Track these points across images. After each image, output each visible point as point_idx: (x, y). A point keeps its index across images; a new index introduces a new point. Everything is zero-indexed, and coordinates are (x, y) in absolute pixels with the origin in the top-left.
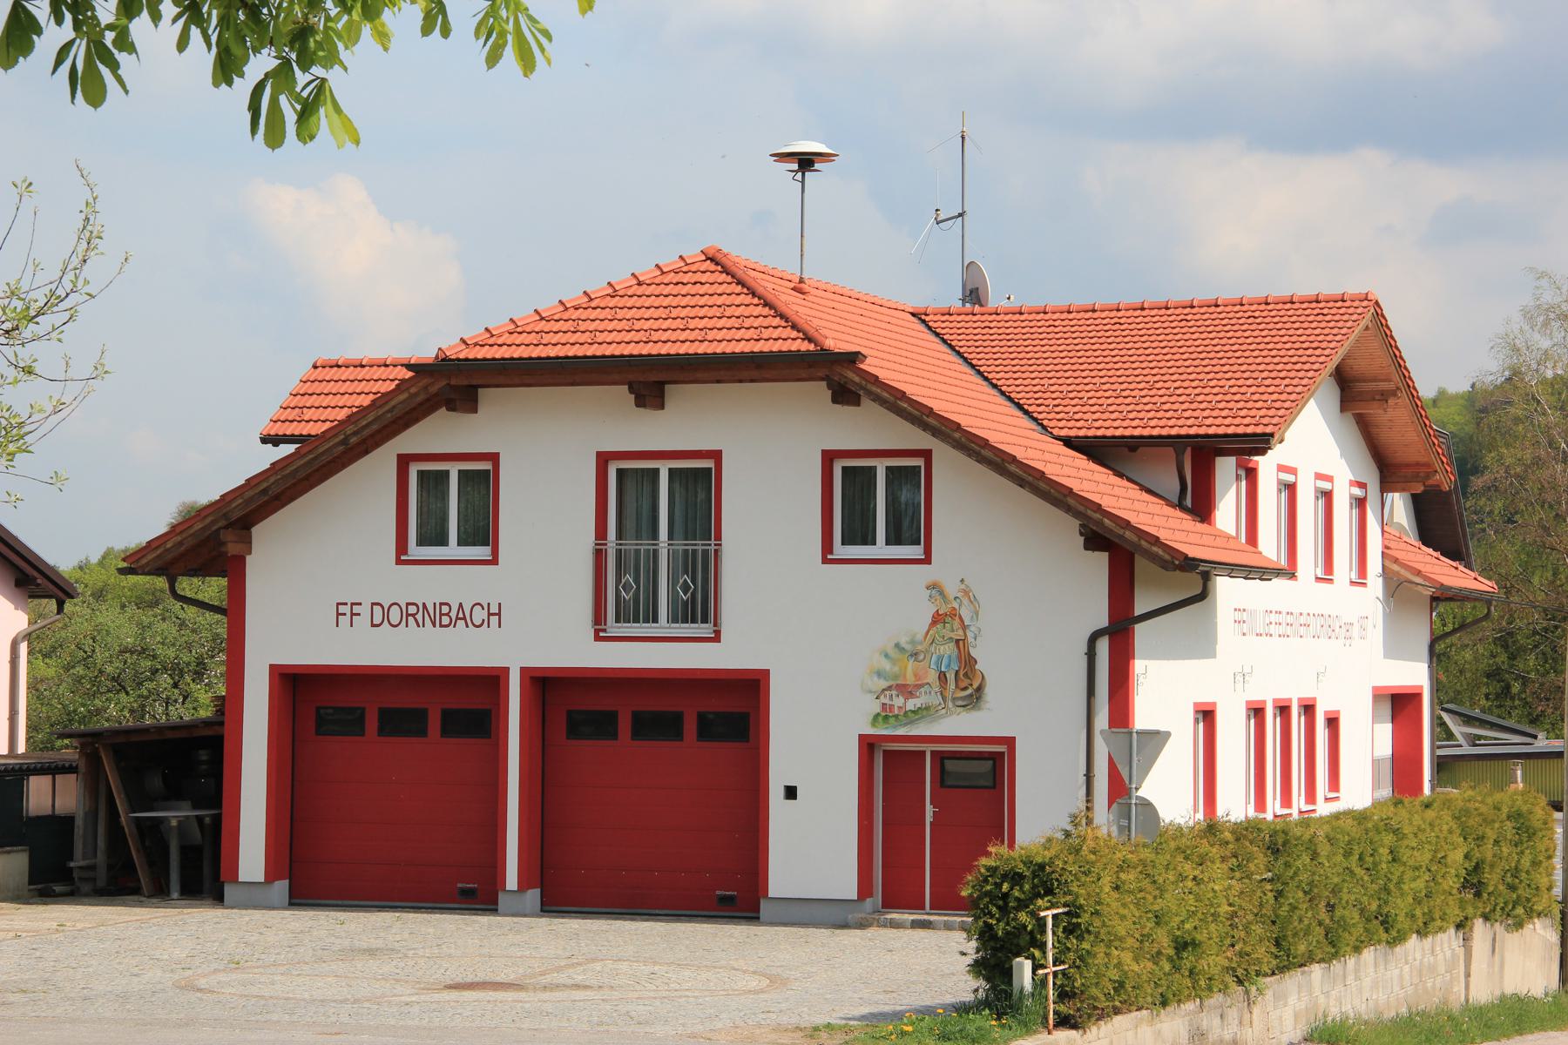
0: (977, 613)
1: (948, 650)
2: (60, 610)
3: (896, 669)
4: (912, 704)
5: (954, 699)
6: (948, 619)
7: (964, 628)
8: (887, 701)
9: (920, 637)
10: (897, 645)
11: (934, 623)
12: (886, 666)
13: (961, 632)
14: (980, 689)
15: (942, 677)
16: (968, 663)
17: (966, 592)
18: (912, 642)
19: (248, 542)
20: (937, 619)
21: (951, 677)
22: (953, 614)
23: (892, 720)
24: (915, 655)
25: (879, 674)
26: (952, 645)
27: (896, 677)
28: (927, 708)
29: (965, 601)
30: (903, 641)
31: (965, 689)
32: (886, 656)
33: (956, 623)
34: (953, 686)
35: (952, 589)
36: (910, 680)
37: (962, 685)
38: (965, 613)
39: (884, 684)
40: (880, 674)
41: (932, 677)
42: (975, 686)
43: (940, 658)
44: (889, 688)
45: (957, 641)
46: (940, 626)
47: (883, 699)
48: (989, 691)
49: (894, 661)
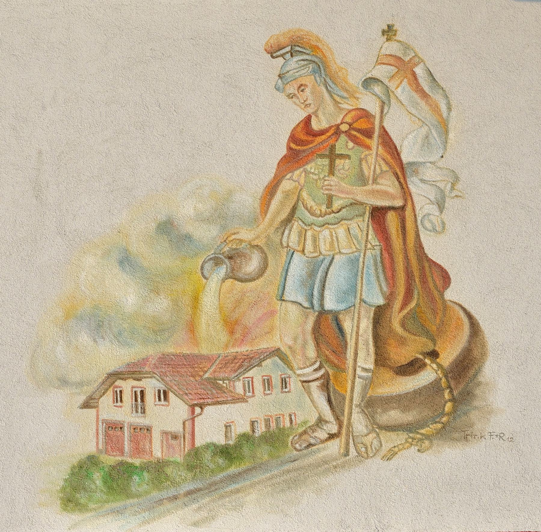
0: (444, 127)
1: (349, 241)
2: (332, 171)
3: (161, 306)
4: (213, 426)
5: (371, 405)
6: (343, 145)
7: (401, 171)
8: (124, 414)
9: (247, 200)
10: (167, 228)
11: (293, 158)
12: (128, 295)
13: (388, 184)
14: (466, 367)
15: (328, 331)
16: (419, 280)
17: (404, 66)
18: (220, 215)
19: (289, 148)
20: (304, 143)
21: (359, 328)
22: (362, 128)
23: (139, 483)
24: (231, 258)
25: (99, 322)
26: (361, 226)
27: (159, 329)
28: (275, 438)
29: (403, 91)
30: (186, 210)
31: (412, 367)
32: (126, 261)
33: (373, 158)
34: (366, 360)
35: (354, 54)
36: (212, 340)
37: (402, 355)
38: (404, 126)
39: (112, 356)
40: (99, 322)
41: (290, 328)
42: (448, 357)
43: (316, 275)
44: (133, 372)
45: (378, 214)
46: (317, 166)
47: (108, 409)
48: (495, 373)
49: (153, 284)
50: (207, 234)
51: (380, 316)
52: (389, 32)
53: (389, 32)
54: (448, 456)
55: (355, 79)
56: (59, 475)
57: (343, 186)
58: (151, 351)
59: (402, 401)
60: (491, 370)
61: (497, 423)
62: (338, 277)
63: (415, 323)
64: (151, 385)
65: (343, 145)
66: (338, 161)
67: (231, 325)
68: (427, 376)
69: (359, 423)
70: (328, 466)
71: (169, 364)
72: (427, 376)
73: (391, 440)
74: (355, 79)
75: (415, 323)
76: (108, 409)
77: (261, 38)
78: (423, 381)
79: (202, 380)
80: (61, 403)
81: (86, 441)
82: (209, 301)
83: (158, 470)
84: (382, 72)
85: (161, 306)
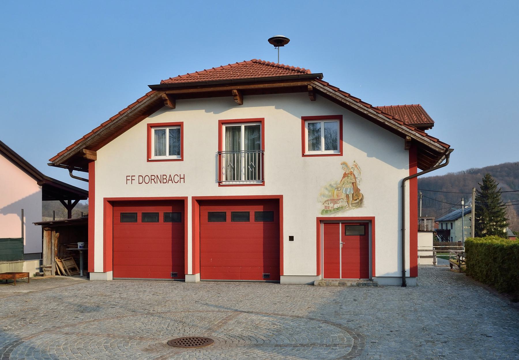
1: (350, 186)
3: (330, 194)
4: (336, 206)
5: (352, 204)
6: (349, 175)
7: (355, 178)
8: (327, 205)
9: (339, 182)
10: (330, 185)
11: (344, 177)
12: (327, 193)
13: (354, 180)
15: (347, 196)
16: (357, 191)
17: (356, 166)
18: (336, 184)
20: (345, 175)
21: (351, 196)
22: (351, 173)
26: (351, 185)
27: (330, 196)
28: (342, 207)
29: (356, 169)
30: (332, 183)
31: (356, 200)
32: (326, 189)
33: (352, 177)
34: (351, 199)
36: (336, 197)
37: (355, 199)
38: (356, 173)
39: (326, 199)
41: (343, 196)
42: (360, 199)
44: (328, 201)
45: (353, 183)
46: (346, 178)
48: (365, 200)
49: (329, 191)
50: (335, 186)
51: (353, 194)
52: (354, 161)
53: (354, 161)
54: (359, 209)
55: (351, 167)
56: (321, 211)
57: (349, 180)
58: (329, 198)
59: (355, 203)
60: (364, 200)
61: (365, 206)
62: (348, 190)
63: (356, 195)
64: (329, 202)
65: (349, 175)
66: (363, 226)
67: (337, 196)
68: (358, 201)
69: (351, 206)
70: (347, 210)
71: (331, 200)
72: (358, 201)
73: (354, 207)
74: (351, 167)
75: (356, 195)
76: (325, 205)
77: (340, 163)
78: (373, 292)
79: (334, 201)
80: (320, 204)
81: (323, 208)
82: (335, 193)
83: (330, 211)
84: (353, 166)
85: (330, 194)
